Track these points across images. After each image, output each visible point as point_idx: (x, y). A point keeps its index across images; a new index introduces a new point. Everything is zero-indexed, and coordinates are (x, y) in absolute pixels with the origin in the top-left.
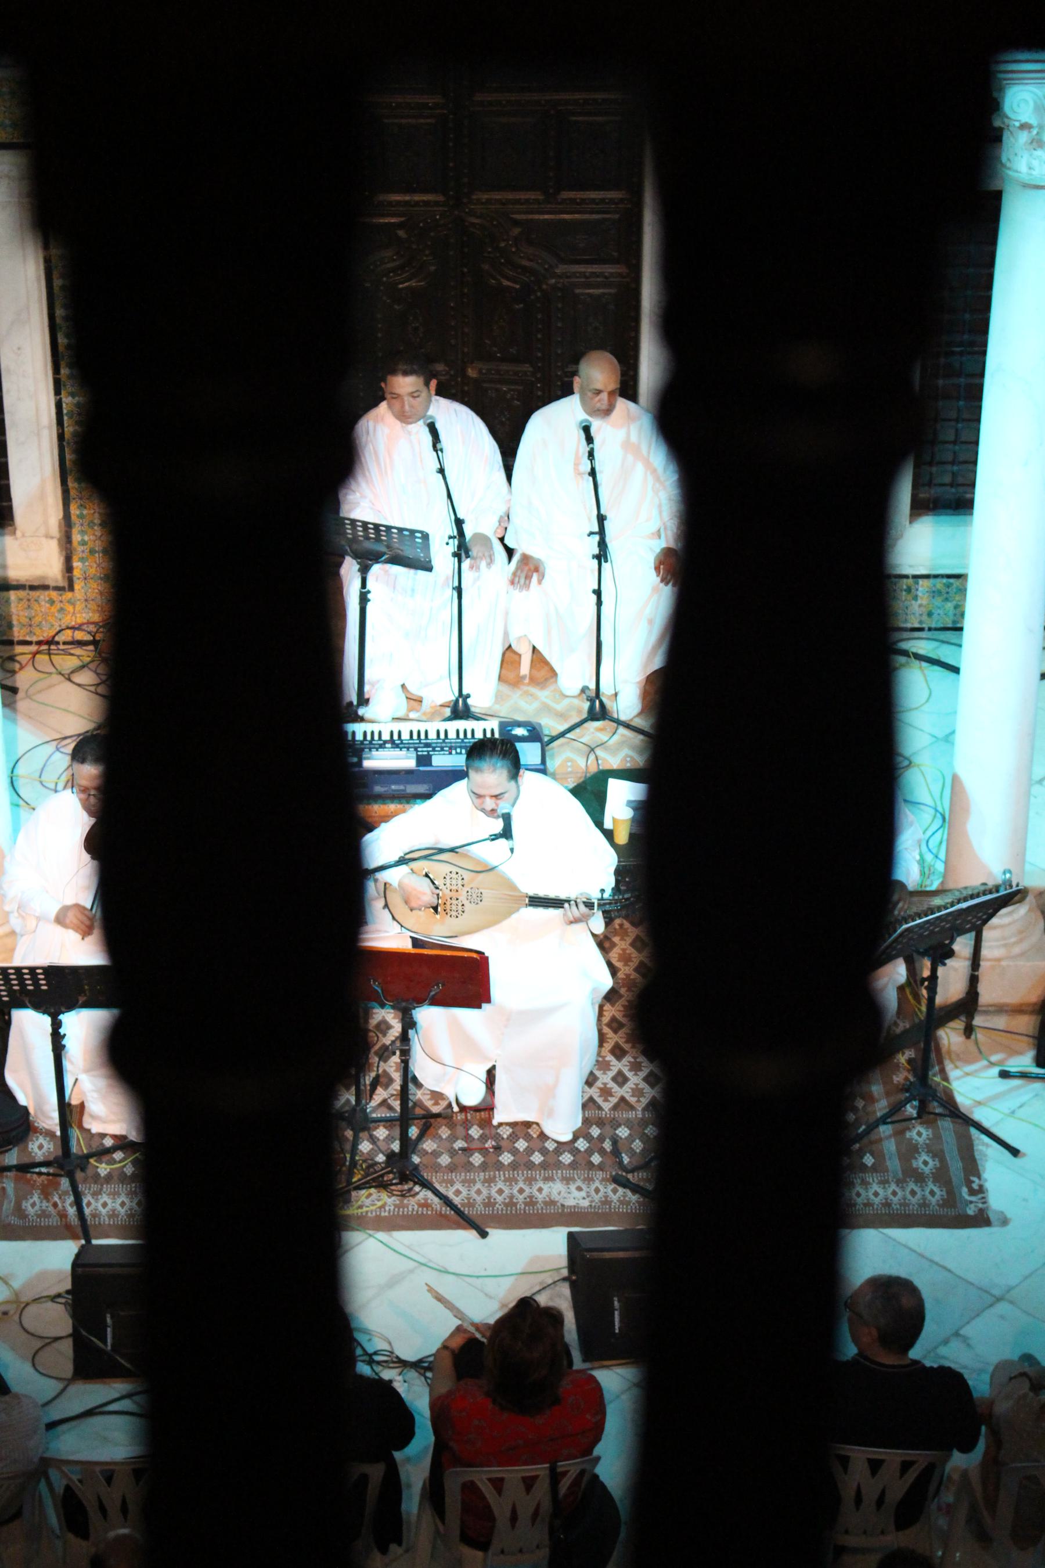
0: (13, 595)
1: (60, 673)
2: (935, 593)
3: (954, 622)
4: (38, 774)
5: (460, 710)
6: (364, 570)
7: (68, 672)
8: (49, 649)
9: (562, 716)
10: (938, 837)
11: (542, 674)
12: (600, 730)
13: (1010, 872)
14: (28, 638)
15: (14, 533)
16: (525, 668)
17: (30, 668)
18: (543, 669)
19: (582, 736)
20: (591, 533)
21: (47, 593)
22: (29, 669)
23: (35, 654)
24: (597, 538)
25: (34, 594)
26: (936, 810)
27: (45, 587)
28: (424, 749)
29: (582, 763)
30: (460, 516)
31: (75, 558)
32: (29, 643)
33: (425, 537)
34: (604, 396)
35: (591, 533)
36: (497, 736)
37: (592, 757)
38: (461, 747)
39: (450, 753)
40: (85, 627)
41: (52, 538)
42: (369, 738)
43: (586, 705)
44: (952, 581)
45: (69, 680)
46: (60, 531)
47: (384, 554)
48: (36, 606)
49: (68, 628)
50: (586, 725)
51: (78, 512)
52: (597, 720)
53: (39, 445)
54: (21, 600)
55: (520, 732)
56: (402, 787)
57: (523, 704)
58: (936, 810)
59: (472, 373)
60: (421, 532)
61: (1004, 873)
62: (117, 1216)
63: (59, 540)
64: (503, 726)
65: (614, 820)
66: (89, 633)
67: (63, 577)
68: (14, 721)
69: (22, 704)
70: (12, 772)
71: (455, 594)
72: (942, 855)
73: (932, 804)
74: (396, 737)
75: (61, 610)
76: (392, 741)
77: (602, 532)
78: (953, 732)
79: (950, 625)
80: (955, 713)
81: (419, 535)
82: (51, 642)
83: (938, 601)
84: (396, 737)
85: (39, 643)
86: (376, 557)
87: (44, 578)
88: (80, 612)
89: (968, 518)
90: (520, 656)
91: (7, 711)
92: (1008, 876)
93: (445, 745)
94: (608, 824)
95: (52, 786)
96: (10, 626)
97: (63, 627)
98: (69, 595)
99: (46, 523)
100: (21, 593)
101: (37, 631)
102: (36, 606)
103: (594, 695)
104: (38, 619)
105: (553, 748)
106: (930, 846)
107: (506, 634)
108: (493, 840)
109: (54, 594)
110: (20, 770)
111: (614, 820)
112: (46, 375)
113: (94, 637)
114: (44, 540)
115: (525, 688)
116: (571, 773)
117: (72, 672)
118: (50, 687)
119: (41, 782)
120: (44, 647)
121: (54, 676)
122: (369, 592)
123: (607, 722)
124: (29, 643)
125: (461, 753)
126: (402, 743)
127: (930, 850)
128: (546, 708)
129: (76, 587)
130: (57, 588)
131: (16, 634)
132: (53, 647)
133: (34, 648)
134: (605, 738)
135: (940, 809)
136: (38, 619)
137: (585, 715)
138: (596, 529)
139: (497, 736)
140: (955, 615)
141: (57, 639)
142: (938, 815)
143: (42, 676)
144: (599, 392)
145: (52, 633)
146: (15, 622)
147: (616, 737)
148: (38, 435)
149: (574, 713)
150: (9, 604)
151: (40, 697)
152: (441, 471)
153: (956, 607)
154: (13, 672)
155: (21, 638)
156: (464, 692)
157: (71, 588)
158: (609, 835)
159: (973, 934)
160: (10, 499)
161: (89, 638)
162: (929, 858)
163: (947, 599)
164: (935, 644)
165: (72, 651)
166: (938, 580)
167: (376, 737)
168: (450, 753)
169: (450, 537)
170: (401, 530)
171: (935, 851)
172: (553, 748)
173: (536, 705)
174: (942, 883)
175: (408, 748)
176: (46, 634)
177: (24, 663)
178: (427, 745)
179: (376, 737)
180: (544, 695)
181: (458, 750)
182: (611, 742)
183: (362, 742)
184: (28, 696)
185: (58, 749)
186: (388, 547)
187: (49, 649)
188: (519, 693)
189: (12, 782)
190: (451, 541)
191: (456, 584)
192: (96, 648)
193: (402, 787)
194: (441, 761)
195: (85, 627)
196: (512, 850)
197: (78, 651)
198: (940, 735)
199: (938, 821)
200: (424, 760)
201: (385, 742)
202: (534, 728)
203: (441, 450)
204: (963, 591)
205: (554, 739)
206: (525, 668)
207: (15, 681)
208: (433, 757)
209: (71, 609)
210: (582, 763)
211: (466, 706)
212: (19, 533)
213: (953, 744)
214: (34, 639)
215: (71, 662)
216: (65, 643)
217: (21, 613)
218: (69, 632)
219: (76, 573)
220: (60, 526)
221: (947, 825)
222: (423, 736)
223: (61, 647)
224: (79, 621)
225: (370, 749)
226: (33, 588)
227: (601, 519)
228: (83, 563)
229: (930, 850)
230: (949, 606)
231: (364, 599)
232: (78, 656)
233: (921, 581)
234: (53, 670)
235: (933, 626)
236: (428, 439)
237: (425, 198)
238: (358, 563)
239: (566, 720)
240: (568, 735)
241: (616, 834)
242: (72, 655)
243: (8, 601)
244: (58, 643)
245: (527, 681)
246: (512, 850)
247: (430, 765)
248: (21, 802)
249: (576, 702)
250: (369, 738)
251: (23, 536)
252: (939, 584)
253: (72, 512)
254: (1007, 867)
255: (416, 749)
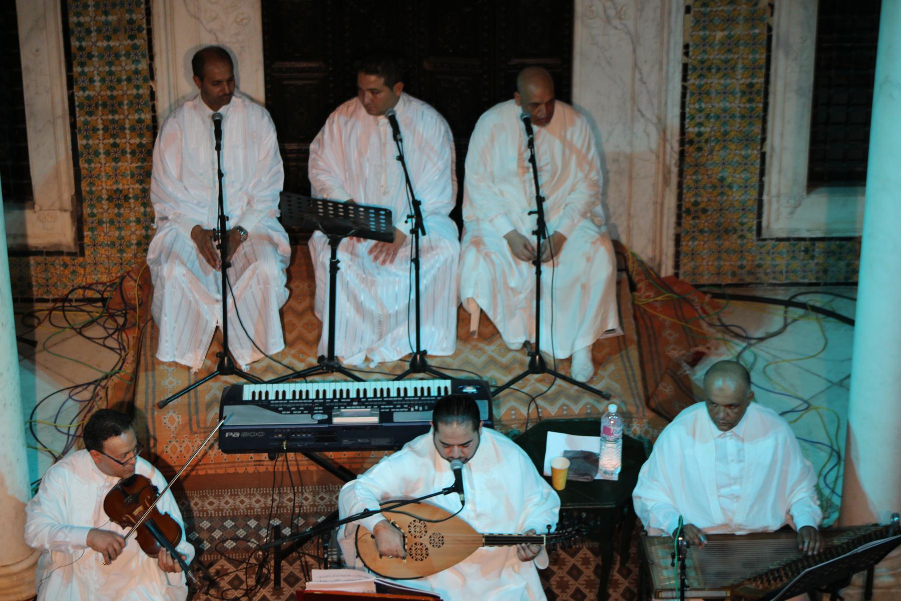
0: (32, 260)
1: (73, 328)
2: (829, 253)
3: (847, 278)
4: (53, 420)
5: (419, 363)
6: (334, 245)
7: (80, 326)
8: (63, 306)
9: (506, 368)
10: (833, 475)
11: (487, 331)
12: (540, 381)
13: (898, 515)
14: (45, 297)
15: (33, 207)
16: (474, 326)
17: (47, 323)
18: (488, 330)
19: (523, 388)
20: (530, 213)
21: (61, 258)
22: (47, 323)
23: (54, 309)
24: (536, 216)
25: (50, 259)
26: (833, 450)
27: (60, 253)
28: (384, 405)
29: (524, 411)
30: (417, 198)
31: (85, 228)
32: (47, 301)
33: (388, 214)
34: (543, 108)
35: (530, 213)
36: (450, 393)
37: (533, 406)
38: (419, 405)
39: (409, 410)
40: (94, 287)
41: (66, 211)
42: (338, 396)
43: (528, 359)
44: (844, 243)
45: (80, 334)
46: (73, 206)
47: (351, 229)
48: (52, 270)
49: (79, 287)
50: (528, 377)
51: (88, 189)
52: (537, 373)
53: (55, 133)
54: (39, 264)
55: (470, 390)
56: (367, 441)
57: (472, 357)
58: (833, 450)
59: (427, 66)
60: (385, 210)
61: (893, 517)
62: (231, 495)
63: (72, 213)
64: (457, 384)
65: (552, 469)
66: (98, 292)
67: (76, 244)
68: (33, 371)
69: (40, 357)
70: (31, 418)
71: (413, 265)
72: (839, 490)
73: (827, 442)
74: (362, 395)
75: (74, 272)
76: (358, 399)
77: (540, 212)
78: (849, 377)
79: (843, 281)
80: (850, 359)
81: (383, 213)
82: (65, 299)
83: (832, 261)
84: (362, 395)
85: (55, 301)
86: (345, 233)
87: (59, 245)
88: (89, 274)
89: (859, 189)
90: (470, 315)
91: (26, 362)
92: (896, 519)
93: (404, 402)
94: (547, 471)
95: (66, 431)
96: (30, 286)
97: (76, 286)
98: (81, 259)
99: (60, 197)
100: (40, 259)
101: (53, 290)
102: (52, 270)
103: (534, 350)
104: (54, 280)
105: (499, 398)
106: (828, 481)
107: (459, 298)
108: (446, 494)
109: (67, 259)
110: (39, 416)
111: (552, 469)
112: (61, 72)
113: (102, 295)
114: (58, 213)
115: (474, 343)
116: (515, 419)
117: (84, 327)
118: (64, 340)
119: (56, 427)
120: (59, 304)
121: (67, 330)
122: (338, 261)
123: (545, 375)
124: (47, 301)
125: (418, 410)
126: (367, 401)
127: (827, 485)
128: (492, 361)
129: (87, 253)
130: (69, 254)
131: (35, 293)
132: (67, 304)
133: (50, 305)
134: (545, 389)
135: (835, 447)
136: (54, 280)
137: (526, 369)
138: (535, 208)
139: (450, 393)
140: (847, 272)
141: (70, 297)
142: (834, 454)
143: (57, 330)
144: (537, 105)
145: (66, 292)
146: (34, 283)
147: (554, 388)
148: (54, 124)
149: (517, 366)
150: (29, 268)
151: (54, 350)
152: (401, 158)
153: (848, 265)
154: (33, 327)
155: (39, 296)
156: (422, 349)
157: (82, 254)
158: (549, 480)
159: (865, 572)
160: (29, 178)
161: (98, 296)
162: (827, 492)
163: (840, 259)
164: (829, 298)
165: (83, 308)
166: (832, 243)
167: (345, 396)
168: (409, 410)
169: (409, 217)
170: (367, 209)
171: (831, 486)
172: (499, 398)
173: (484, 358)
174: (839, 519)
175: (372, 406)
176: (62, 292)
177: (42, 318)
178: (389, 403)
179: (345, 396)
180: (491, 349)
181: (416, 408)
182: (549, 392)
183: (332, 400)
184: (45, 349)
185: (70, 397)
186: (354, 222)
187: (63, 306)
188: (469, 346)
189: (31, 427)
190: (410, 220)
191: (414, 256)
192: (104, 306)
193: (367, 441)
194: (401, 417)
195: (94, 287)
196: (463, 503)
197: (88, 308)
198: (835, 380)
199: (834, 460)
200: (386, 417)
201: (353, 400)
202: (482, 387)
203: (401, 140)
204: (857, 254)
205: (500, 389)
206: (474, 326)
207: (34, 335)
208: (395, 414)
209: (82, 271)
210: (524, 411)
211: (423, 361)
212: (37, 208)
213: (848, 389)
214: (51, 297)
215: (83, 318)
216: (77, 301)
217: (39, 275)
218: (81, 291)
219: (86, 241)
220: (72, 201)
221: (842, 463)
222: (385, 395)
223: (74, 304)
224: (89, 281)
225: (339, 407)
226: (49, 254)
227: (540, 200)
228: (92, 232)
229: (827, 485)
230: (842, 264)
231: (334, 268)
232: (88, 312)
233: (817, 244)
234: (66, 325)
235: (828, 281)
236: (390, 130)
237: (310, 65)
238: (329, 237)
239: (510, 373)
240: (512, 386)
241: (555, 481)
242: (84, 311)
243: (28, 265)
244: (71, 301)
245: (476, 336)
246: (463, 503)
247: (391, 420)
248: (39, 446)
249: (519, 355)
250: (338, 396)
251: (41, 209)
252: (833, 245)
253: (83, 189)
254: (896, 511)
255: (379, 406)
